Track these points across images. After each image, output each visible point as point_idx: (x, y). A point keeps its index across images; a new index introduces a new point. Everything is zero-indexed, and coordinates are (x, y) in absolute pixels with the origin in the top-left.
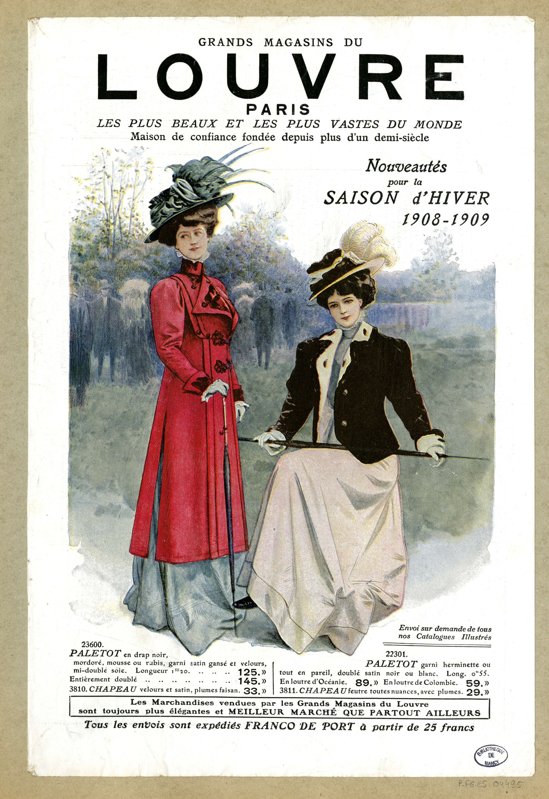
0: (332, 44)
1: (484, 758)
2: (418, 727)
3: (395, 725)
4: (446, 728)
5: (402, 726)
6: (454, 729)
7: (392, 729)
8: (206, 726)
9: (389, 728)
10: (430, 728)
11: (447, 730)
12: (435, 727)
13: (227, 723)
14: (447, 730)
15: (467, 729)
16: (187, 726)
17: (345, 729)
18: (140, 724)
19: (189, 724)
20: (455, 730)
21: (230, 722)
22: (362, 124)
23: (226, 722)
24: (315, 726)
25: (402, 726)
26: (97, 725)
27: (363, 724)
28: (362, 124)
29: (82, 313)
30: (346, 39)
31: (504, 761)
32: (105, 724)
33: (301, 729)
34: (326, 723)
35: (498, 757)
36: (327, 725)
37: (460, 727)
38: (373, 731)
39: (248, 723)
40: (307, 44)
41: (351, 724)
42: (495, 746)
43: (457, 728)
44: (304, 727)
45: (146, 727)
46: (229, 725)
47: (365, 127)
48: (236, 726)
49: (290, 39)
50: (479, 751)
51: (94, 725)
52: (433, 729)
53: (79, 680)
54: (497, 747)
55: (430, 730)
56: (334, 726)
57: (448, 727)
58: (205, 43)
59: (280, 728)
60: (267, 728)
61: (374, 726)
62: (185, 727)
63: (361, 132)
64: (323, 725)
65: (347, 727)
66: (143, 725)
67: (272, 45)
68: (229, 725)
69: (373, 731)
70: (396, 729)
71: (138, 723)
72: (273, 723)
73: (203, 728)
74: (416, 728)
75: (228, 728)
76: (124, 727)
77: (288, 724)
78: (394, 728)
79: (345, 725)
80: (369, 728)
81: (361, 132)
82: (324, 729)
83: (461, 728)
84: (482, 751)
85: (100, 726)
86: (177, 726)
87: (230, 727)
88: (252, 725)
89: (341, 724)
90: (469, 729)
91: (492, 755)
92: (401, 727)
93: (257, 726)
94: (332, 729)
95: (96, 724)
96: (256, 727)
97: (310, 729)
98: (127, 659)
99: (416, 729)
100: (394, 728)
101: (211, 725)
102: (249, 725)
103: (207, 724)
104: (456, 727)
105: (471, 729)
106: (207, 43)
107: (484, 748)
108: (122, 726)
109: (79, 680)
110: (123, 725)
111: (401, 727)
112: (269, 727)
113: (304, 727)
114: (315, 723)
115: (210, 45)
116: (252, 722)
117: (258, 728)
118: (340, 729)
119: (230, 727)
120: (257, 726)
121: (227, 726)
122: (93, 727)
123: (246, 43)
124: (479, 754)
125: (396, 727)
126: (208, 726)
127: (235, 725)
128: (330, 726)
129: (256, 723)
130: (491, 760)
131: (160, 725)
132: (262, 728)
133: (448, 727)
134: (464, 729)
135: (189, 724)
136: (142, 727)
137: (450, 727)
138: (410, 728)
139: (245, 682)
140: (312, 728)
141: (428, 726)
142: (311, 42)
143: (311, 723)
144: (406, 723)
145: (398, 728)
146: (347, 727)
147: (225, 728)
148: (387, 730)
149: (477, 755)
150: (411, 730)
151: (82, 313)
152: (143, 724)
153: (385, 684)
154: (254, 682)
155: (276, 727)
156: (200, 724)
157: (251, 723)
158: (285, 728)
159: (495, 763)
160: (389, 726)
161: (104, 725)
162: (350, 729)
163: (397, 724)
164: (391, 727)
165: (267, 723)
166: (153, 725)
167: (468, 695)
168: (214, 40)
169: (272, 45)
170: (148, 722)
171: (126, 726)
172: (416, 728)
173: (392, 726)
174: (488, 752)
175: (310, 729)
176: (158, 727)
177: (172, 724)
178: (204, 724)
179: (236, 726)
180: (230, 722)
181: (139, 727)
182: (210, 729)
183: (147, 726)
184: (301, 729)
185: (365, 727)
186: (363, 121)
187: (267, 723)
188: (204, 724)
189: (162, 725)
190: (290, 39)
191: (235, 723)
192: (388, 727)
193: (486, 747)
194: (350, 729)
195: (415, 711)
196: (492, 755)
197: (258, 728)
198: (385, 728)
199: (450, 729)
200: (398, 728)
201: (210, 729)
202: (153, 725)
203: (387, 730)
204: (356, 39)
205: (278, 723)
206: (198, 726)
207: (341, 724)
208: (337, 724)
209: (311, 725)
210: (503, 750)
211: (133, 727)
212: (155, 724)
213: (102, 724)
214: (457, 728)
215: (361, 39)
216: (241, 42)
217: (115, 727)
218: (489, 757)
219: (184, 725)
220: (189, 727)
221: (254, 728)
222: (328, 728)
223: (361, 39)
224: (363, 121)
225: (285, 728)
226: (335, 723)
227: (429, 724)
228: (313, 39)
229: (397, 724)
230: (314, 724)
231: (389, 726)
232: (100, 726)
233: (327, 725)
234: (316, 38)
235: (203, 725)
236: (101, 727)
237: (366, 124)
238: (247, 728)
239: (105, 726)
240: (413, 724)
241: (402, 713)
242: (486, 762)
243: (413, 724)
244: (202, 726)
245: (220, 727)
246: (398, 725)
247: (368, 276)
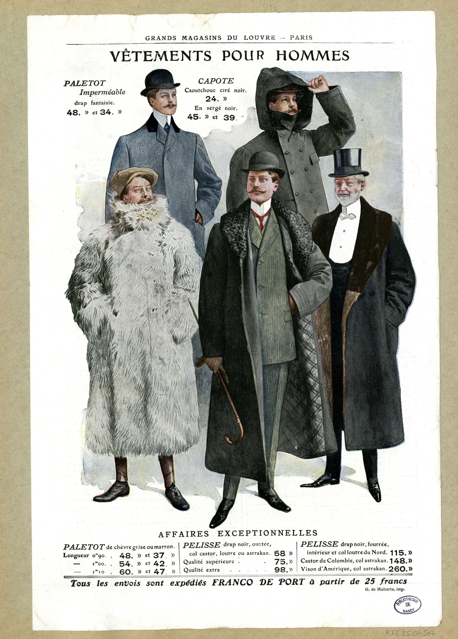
0: (221, 39)
1: (402, 607)
2: (359, 581)
3: (338, 580)
4: (384, 582)
5: (344, 581)
6: (390, 582)
7: (336, 583)
8: (179, 584)
9: (334, 583)
10: (370, 582)
11: (385, 583)
12: (374, 581)
13: (196, 581)
14: (385, 583)
15: (401, 582)
16: (160, 584)
17: (297, 584)
18: (120, 583)
19: (162, 582)
20: (392, 583)
21: (197, 580)
22: (227, 81)
23: (194, 580)
24: (272, 582)
25: (344, 581)
26: (81, 584)
27: (312, 579)
28: (227, 81)
30: (228, 36)
31: (400, 613)
32: (88, 583)
33: (261, 584)
34: (281, 579)
35: (414, 606)
36: (283, 580)
37: (395, 581)
38: (321, 585)
39: (214, 580)
40: (207, 39)
41: (302, 579)
42: (410, 597)
43: (393, 582)
44: (263, 583)
45: (126, 585)
46: (197, 582)
47: (229, 83)
48: (203, 583)
49: (197, 36)
50: (398, 602)
51: (79, 584)
52: (372, 582)
53: (312, 553)
54: (412, 597)
55: (369, 583)
56: (288, 582)
57: (386, 581)
58: (149, 39)
59: (241, 584)
60: (230, 584)
61: (322, 581)
62: (159, 585)
64: (279, 580)
66: (123, 584)
67: (186, 40)
68: (197, 582)
69: (321, 585)
70: (339, 584)
71: (394, 580)
72: (235, 580)
73: (175, 585)
74: (357, 582)
75: (196, 585)
76: (105, 585)
77: (247, 580)
78: (337, 582)
79: (297, 581)
80: (317, 582)
82: (281, 584)
83: (396, 581)
84: (400, 601)
85: (84, 584)
86: (153, 584)
87: (198, 584)
88: (218, 582)
89: (294, 579)
90: (402, 582)
91: (408, 605)
92: (343, 581)
93: (296, 582)
94: (287, 584)
95: (80, 583)
96: (295, 583)
97: (268, 584)
99: (357, 583)
100: (337, 582)
101: (182, 582)
102: (216, 582)
103: (179, 582)
104: (392, 581)
105: (404, 582)
106: (151, 39)
107: (402, 599)
108: (103, 584)
109: (312, 553)
110: (104, 584)
111: (343, 581)
112: (232, 583)
113: (263, 583)
114: (272, 579)
115: (152, 40)
116: (218, 580)
117: (223, 585)
118: (293, 584)
119: (198, 584)
120: (296, 582)
121: (195, 583)
122: (78, 585)
123: (172, 38)
124: (398, 604)
125: (339, 581)
126: (180, 584)
127: (202, 582)
128: (285, 582)
129: (221, 580)
130: (408, 608)
131: (137, 584)
132: (226, 585)
133: (386, 581)
134: (398, 582)
135: (162, 582)
136: (123, 585)
137: (388, 580)
138: (352, 582)
139: (395, 562)
140: (270, 583)
141: (368, 580)
142: (209, 38)
143: (269, 580)
145: (340, 582)
146: (299, 582)
147: (193, 585)
148: (331, 584)
149: (396, 605)
150: (353, 583)
152: (123, 583)
153: (219, 536)
154: (401, 554)
155: (237, 583)
156: (174, 582)
157: (217, 580)
158: (245, 584)
159: (412, 610)
160: (334, 581)
161: (87, 584)
162: (301, 584)
163: (340, 579)
164: (335, 581)
165: (230, 580)
166: (131, 584)
168: (154, 37)
169: (186, 40)
170: (127, 581)
171: (107, 585)
172: (357, 582)
173: (336, 580)
174: (405, 602)
175: (268, 584)
176: (135, 585)
177: (148, 583)
178: (177, 582)
179: (203, 583)
180: (197, 580)
181: (120, 585)
182: (181, 586)
183: (126, 584)
184: (261, 584)
185: (313, 581)
186: (227, 79)
187: (230, 580)
188: (177, 582)
189: (138, 583)
190: (197, 36)
191: (202, 580)
192: (332, 581)
193: (403, 598)
194: (301, 584)
195: (194, 52)
196: (408, 605)
197: (223, 585)
198: (330, 582)
199: (387, 582)
200: (340, 582)
201: (181, 586)
202: (131, 584)
203: (331, 584)
204: (234, 36)
205: (239, 580)
207: (294, 579)
208: (290, 580)
209: (269, 581)
210: (417, 600)
211: (115, 585)
212: (132, 583)
213: (85, 583)
214: (393, 582)
215: (236, 36)
216: (170, 38)
217: (98, 585)
218: (406, 606)
219: (158, 583)
220: (162, 585)
221: (220, 585)
222: (284, 584)
223: (236, 36)
224: (227, 79)
225: (245, 584)
226: (289, 579)
227: (369, 579)
228: (210, 36)
229: (340, 579)
230: (271, 580)
231: (334, 581)
232: (84, 584)
233: (283, 580)
234: (212, 35)
235: (176, 583)
236: (85, 585)
237: (230, 81)
238: (214, 585)
239: (138, 585)
240: (354, 579)
241: (403, 569)
242: (404, 610)
243: (354, 579)
244: (175, 583)
245: (189, 584)
246: (341, 580)
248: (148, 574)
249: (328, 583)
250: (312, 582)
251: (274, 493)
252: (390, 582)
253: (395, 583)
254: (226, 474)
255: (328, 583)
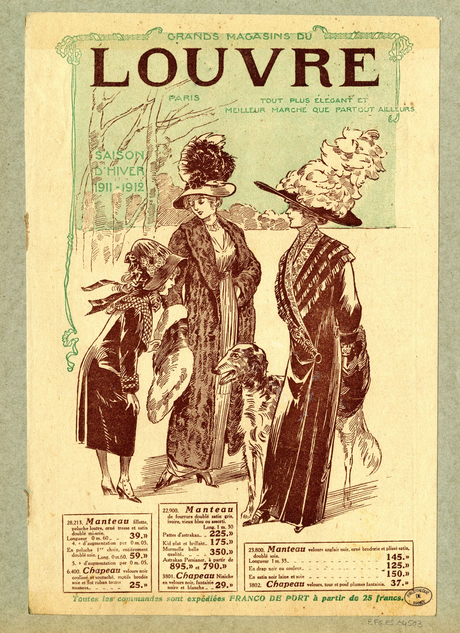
3: (339, 596)
7: (336, 600)
9: (334, 599)
29: (359, 504)
41: (306, 596)
43: (281, 550)
44: (272, 599)
63: (111, 525)
65: (304, 599)
72: (249, 597)
78: (338, 599)
80: (320, 599)
81: (111, 525)
87: (212, 600)
97: (277, 600)
98: (98, 526)
100: (338, 599)
119: (212, 600)
125: (340, 598)
139: (392, 558)
144: (348, 595)
146: (304, 599)
151: (359, 504)
167: (131, 587)
175: (277, 600)
206: (189, 600)
214: (281, 550)
232: (212, 576)
247: (300, 525)
248: (183, 590)
249: (330, 599)
250: (316, 599)
251: (301, 437)
252: (112, 571)
253: (103, 523)
254: (28, 10)
255: (330, 599)
